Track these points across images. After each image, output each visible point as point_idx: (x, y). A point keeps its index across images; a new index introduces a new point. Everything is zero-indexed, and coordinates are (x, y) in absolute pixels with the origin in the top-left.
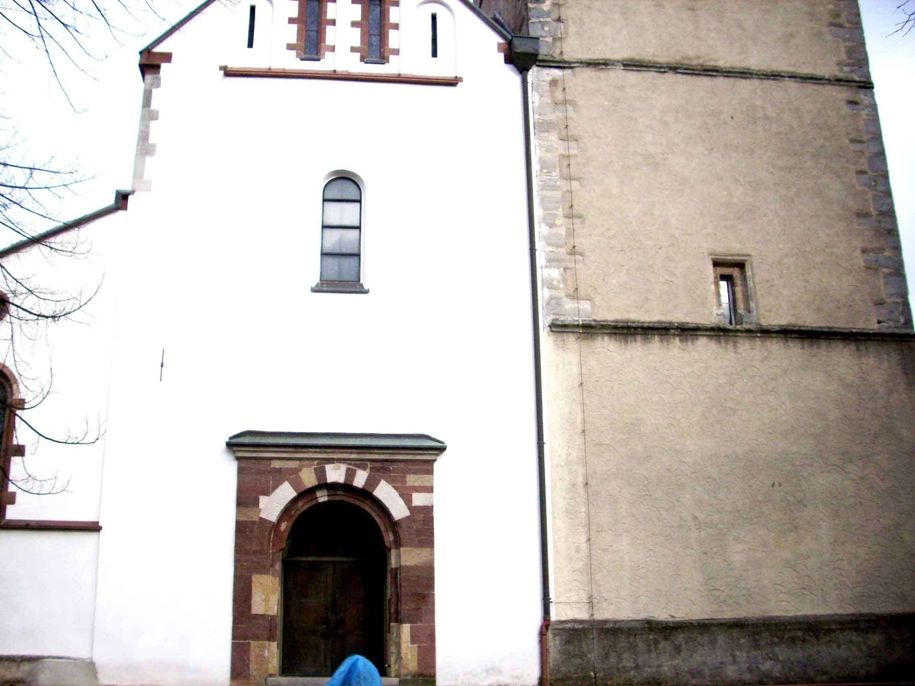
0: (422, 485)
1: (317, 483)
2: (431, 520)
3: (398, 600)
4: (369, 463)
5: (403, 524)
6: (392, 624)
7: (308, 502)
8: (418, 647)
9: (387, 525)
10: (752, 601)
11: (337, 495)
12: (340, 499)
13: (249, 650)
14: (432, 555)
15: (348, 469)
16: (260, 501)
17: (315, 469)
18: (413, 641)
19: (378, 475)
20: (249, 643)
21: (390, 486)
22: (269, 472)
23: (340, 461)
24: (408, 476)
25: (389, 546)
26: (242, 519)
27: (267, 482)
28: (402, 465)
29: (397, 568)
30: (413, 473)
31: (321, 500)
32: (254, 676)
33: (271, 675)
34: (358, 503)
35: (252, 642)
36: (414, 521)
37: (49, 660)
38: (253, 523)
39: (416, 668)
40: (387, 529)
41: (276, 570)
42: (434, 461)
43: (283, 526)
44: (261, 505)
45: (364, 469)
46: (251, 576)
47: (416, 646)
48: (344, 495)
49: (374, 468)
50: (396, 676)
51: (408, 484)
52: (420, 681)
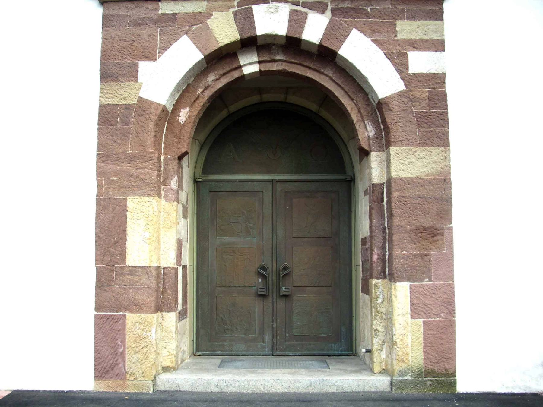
0: (425, 37)
1: (238, 37)
5: (395, 105)
7: (224, 74)
8: (424, 322)
11: (274, 61)
13: (124, 329)
14: (447, 158)
15: (293, 13)
17: (235, 14)
19: (345, 22)
20: (125, 316)
24: (399, 22)
25: (366, 148)
26: (110, 102)
27: (153, 37)
30: (408, 18)
31: (248, 70)
32: (133, 374)
33: (166, 369)
34: (310, 74)
35: (128, 315)
37: (220, 193)
38: (128, 107)
39: (422, 362)
40: (362, 117)
41: (171, 189)
43: (183, 115)
45: (323, 11)
46: (125, 200)
47: (420, 321)
48: (286, 61)
49: (339, 9)
50: (384, 372)
51: (399, 37)
52: (429, 383)
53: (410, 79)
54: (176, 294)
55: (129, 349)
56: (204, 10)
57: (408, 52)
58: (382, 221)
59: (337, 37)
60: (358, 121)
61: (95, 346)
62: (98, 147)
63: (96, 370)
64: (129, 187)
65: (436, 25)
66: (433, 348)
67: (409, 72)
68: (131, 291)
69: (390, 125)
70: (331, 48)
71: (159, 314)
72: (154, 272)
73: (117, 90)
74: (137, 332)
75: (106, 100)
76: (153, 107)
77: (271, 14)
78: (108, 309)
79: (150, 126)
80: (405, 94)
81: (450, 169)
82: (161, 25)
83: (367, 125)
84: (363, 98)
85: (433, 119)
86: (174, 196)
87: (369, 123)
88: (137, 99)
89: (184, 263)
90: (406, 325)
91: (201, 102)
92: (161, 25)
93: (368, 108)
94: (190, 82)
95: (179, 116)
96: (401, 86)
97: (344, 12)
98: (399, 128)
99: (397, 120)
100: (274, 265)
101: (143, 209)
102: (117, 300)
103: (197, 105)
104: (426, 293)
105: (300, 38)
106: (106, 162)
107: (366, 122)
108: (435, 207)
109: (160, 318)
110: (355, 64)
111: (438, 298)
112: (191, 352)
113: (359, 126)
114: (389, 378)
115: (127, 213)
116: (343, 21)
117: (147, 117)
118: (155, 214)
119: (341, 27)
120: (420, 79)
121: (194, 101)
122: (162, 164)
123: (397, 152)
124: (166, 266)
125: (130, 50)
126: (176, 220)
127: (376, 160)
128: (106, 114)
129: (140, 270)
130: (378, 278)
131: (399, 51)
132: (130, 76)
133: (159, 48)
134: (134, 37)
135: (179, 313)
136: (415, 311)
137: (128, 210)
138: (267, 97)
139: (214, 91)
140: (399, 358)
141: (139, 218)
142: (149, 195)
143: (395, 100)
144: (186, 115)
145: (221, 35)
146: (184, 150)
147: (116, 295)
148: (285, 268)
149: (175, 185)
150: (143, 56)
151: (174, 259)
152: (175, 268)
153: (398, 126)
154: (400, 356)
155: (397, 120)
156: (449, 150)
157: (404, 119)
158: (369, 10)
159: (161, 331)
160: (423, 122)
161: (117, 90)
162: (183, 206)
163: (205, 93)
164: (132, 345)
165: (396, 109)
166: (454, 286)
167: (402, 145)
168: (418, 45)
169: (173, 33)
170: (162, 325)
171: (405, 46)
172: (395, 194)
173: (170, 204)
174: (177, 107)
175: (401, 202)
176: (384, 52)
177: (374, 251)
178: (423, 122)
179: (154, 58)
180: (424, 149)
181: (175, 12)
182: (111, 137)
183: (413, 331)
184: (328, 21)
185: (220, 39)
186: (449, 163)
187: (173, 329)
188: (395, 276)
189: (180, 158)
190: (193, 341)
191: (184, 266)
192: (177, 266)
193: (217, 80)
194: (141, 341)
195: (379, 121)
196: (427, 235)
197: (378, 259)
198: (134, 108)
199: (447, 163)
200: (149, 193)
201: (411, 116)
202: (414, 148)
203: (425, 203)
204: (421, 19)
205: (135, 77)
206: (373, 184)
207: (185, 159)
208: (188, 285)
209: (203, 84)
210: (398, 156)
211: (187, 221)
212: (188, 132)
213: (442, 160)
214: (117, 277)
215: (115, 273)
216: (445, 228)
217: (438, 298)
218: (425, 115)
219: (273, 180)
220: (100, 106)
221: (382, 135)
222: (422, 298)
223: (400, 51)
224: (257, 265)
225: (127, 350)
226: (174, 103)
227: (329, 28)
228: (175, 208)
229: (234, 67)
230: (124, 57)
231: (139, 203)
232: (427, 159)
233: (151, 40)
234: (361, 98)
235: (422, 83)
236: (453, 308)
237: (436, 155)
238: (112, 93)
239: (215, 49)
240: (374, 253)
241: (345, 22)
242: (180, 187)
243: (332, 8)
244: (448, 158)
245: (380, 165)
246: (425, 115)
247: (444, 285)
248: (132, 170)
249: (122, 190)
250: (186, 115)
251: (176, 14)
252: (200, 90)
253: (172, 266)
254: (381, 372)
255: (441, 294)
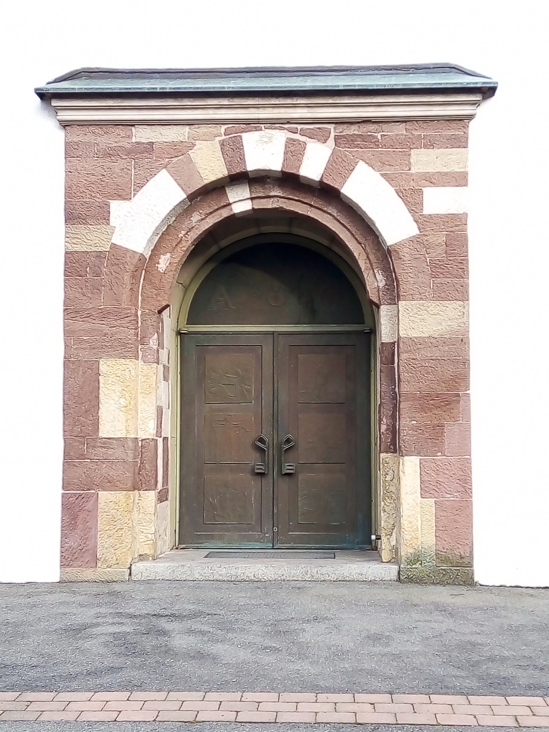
0: (446, 170)
2: (463, 241)
3: (395, 408)
4: (332, 127)
5: (406, 253)
6: (383, 455)
9: (372, 257)
10: (430, 275)
12: (275, 206)
14: (465, 314)
15: (290, 142)
16: (112, 210)
17: (222, 144)
18: (425, 492)
19: (351, 152)
21: (377, 175)
22: (129, 152)
23: (272, 123)
25: (376, 300)
26: (78, 248)
28: (400, 130)
29: (394, 343)
30: (425, 147)
33: (142, 557)
36: (428, 247)
38: (99, 255)
41: (150, 349)
42: (471, 117)
44: (113, 220)
53: (425, 221)
54: (156, 471)
55: (101, 533)
56: (185, 139)
57: (423, 189)
58: (392, 386)
59: (341, 173)
60: (366, 269)
61: (62, 530)
62: (65, 301)
63: (63, 557)
64: (102, 348)
65: (458, 154)
66: (446, 532)
67: (424, 213)
68: (104, 466)
69: (399, 276)
70: (333, 185)
71: (136, 492)
72: (131, 444)
73: (86, 235)
74: (110, 513)
75: (73, 245)
76: (128, 255)
77: (264, 144)
78: (78, 486)
79: (126, 278)
80: (418, 240)
81: (468, 327)
82: (136, 156)
83: (377, 274)
84: (372, 242)
85: (450, 268)
86: (153, 357)
87: (379, 271)
88: (110, 246)
89: (165, 435)
90: (415, 504)
91: (184, 247)
92: (136, 156)
93: (378, 254)
94: (171, 223)
95: (158, 263)
96: (413, 230)
97: (349, 139)
98: (410, 279)
99: (408, 270)
100: (275, 437)
101: (119, 373)
102: (88, 476)
103: (179, 250)
104: (438, 469)
105: (297, 173)
106: (75, 319)
107: (376, 271)
108: (449, 371)
109: (137, 498)
110: (360, 205)
111: (453, 475)
112: (173, 544)
113: (368, 274)
114: (397, 567)
115: (100, 377)
116: (347, 151)
117: (122, 266)
118: (133, 379)
119: (345, 159)
120: (437, 221)
121: (176, 245)
122: (140, 319)
123: (407, 308)
124: (144, 437)
125: (100, 186)
126: (156, 384)
127: (387, 315)
128: (74, 263)
129: (114, 441)
130: (387, 452)
131: (412, 188)
132: (101, 218)
133: (134, 185)
134: (103, 171)
135: (159, 493)
136: (426, 489)
137: (101, 374)
138: (265, 229)
139: (199, 233)
140: (407, 543)
141: (113, 383)
142: (125, 357)
143: (406, 247)
144: (167, 262)
145: (206, 170)
146: (164, 304)
147: (87, 471)
148: (288, 441)
149: (155, 344)
150: (115, 194)
151: (154, 429)
152: (155, 439)
153: (409, 277)
154: (408, 541)
155: (408, 270)
156: (468, 304)
157: (416, 269)
158: (379, 137)
159: (138, 512)
160: (438, 272)
161: (86, 235)
162: (164, 366)
163: (188, 235)
164: (105, 527)
165: (407, 257)
166: (471, 461)
167: (413, 299)
168: (435, 179)
169: (150, 167)
170: (139, 506)
171: (421, 181)
172: (403, 355)
173: (148, 366)
174: (156, 251)
175: (410, 365)
176: (395, 190)
177: (383, 421)
178: (438, 272)
179: (128, 197)
180: (439, 304)
181: (151, 141)
182: (80, 290)
183: (423, 513)
184: (331, 152)
185: (205, 175)
186: (468, 319)
187: (152, 510)
188: (403, 449)
189: (160, 312)
190: (175, 531)
191: (165, 438)
192: (156, 438)
193: (202, 219)
194: (116, 523)
195: (391, 269)
196: (442, 402)
197: (387, 430)
198: (106, 256)
199: (465, 320)
200: (125, 355)
201: (424, 265)
202: (427, 303)
203: (439, 366)
204: (441, 147)
205: (106, 219)
206: (382, 343)
207: (166, 313)
208: (169, 461)
209: (186, 224)
210: (408, 312)
211: (169, 384)
212: (170, 279)
213: (459, 316)
214: (88, 450)
215: (86, 445)
216: (461, 395)
217: (453, 475)
218: (441, 263)
219: (273, 332)
220: (66, 253)
221: (394, 286)
222: (433, 474)
223: (414, 187)
224: (254, 435)
225: (99, 533)
226: (152, 247)
227: (331, 161)
228: (155, 371)
229: (222, 204)
230: (93, 195)
231: (113, 366)
232: (442, 316)
233: (124, 175)
234: (371, 242)
235: (439, 226)
236: (470, 487)
237: (453, 311)
238: (79, 237)
239: (199, 187)
240: (382, 422)
241: (351, 152)
242: (160, 344)
243: (335, 136)
244: (466, 313)
245: (391, 320)
246: (441, 263)
247: (459, 460)
248: (106, 329)
249: (94, 351)
250: (167, 262)
251: (153, 143)
252: (183, 232)
253: (151, 437)
254: (390, 561)
255: (456, 471)
